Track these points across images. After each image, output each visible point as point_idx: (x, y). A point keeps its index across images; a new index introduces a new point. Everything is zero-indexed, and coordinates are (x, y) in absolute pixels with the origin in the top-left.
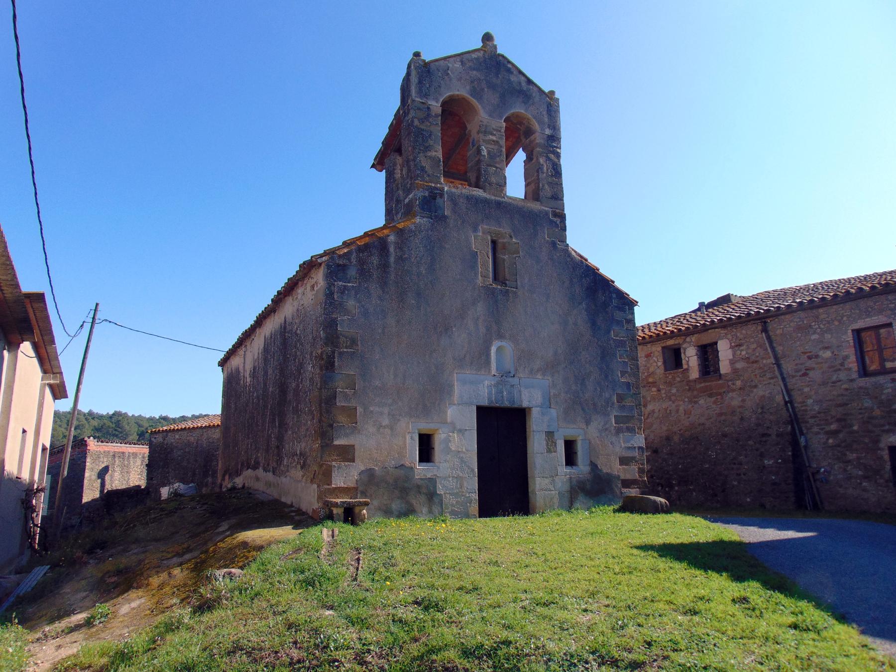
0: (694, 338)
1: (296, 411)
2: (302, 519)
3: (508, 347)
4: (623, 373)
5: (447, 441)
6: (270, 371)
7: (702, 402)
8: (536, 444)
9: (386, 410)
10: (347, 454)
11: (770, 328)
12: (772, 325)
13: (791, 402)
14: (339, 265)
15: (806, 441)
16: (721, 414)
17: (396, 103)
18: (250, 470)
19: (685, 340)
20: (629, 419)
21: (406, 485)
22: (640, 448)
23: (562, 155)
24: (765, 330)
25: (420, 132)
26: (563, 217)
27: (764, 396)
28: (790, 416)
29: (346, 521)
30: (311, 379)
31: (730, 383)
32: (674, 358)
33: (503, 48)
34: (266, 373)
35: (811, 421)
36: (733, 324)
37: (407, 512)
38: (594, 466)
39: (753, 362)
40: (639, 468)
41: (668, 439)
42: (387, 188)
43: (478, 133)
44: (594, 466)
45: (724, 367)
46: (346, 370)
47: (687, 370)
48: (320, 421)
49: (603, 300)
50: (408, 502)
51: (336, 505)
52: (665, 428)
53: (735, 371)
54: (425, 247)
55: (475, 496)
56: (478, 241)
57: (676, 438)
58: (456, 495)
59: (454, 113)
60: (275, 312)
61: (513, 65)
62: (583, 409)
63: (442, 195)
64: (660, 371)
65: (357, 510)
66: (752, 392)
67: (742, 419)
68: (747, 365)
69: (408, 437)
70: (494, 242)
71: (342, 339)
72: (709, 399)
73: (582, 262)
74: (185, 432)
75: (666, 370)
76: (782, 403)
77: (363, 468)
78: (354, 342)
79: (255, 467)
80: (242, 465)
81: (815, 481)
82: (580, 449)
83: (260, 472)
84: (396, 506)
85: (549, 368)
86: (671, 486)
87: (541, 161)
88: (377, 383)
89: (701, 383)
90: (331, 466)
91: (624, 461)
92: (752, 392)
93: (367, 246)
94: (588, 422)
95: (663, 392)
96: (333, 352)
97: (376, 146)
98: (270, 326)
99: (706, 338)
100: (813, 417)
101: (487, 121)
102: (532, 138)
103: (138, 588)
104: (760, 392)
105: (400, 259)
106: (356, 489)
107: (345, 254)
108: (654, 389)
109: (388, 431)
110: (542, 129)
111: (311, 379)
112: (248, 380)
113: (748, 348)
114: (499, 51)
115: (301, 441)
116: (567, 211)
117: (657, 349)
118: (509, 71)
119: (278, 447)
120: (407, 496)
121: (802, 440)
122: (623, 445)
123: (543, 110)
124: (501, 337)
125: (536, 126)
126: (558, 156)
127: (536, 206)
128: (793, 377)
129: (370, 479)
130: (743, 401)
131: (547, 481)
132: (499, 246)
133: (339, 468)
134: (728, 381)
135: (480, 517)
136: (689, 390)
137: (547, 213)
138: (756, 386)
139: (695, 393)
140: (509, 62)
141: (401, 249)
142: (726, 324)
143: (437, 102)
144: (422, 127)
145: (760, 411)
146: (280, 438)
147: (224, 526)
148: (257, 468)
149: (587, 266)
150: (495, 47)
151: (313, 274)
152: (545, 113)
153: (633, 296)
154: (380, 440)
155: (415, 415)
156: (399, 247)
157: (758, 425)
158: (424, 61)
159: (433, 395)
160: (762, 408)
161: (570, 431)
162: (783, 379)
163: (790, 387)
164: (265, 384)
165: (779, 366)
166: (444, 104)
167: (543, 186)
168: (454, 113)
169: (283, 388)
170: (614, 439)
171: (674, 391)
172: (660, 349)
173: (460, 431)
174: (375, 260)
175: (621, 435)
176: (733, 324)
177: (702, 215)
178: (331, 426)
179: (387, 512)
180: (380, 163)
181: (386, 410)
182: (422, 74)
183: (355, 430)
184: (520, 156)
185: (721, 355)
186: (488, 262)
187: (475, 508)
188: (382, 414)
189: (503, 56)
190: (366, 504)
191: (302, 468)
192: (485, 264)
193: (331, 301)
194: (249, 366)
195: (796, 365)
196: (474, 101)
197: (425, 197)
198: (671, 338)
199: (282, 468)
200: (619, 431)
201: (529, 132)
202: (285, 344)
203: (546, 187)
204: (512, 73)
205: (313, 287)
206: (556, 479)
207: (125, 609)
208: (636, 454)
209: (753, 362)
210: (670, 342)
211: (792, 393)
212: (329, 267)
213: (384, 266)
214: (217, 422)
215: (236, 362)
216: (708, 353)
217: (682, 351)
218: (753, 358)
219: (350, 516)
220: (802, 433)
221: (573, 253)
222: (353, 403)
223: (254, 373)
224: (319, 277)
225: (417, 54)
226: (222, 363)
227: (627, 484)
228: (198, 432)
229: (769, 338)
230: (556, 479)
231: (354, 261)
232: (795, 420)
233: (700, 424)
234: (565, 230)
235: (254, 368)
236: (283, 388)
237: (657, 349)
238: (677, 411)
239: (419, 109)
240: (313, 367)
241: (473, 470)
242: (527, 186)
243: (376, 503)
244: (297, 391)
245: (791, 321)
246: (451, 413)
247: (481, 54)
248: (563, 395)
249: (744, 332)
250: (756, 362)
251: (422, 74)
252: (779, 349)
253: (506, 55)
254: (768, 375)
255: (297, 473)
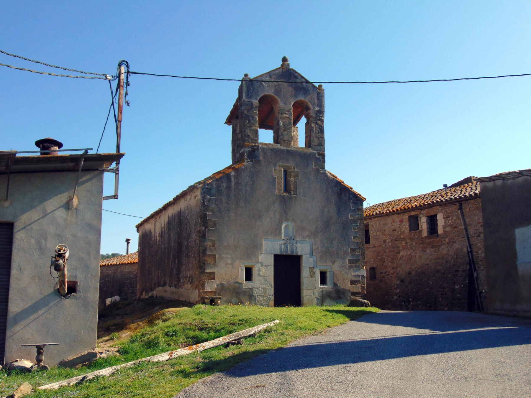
0: (425, 211)
1: (187, 256)
2: (190, 305)
3: (291, 225)
4: (355, 237)
5: (259, 270)
6: (172, 235)
7: (428, 251)
8: (305, 273)
9: (229, 256)
10: (212, 276)
11: (463, 207)
12: (465, 206)
13: (471, 252)
14: (207, 188)
15: (477, 275)
16: (437, 258)
17: (237, 96)
18: (160, 288)
19: (420, 212)
20: (356, 261)
21: (239, 291)
22: (362, 276)
23: (325, 121)
24: (460, 209)
25: (247, 117)
26: (323, 155)
27: (458, 248)
28: (470, 260)
29: (211, 304)
30: (195, 241)
31: (443, 240)
32: (414, 222)
33: (293, 65)
34: (169, 235)
35: (480, 263)
36: (453, 202)
37: (241, 303)
38: (335, 285)
39: (454, 228)
40: (362, 287)
41: (409, 273)
42: (233, 137)
43: (279, 113)
44: (335, 285)
45: (440, 230)
46: (211, 237)
47: (421, 230)
48: (199, 261)
49: (346, 197)
50: (239, 299)
51: (207, 298)
52: (408, 267)
53: (445, 232)
54: (249, 176)
55: (272, 297)
56: (277, 172)
57: (413, 273)
58: (263, 296)
59: (267, 103)
60: (174, 204)
61: (298, 73)
62: (331, 256)
63: (258, 149)
64: (407, 231)
65: (216, 301)
66: (453, 245)
67: (447, 261)
68: (451, 229)
69: (240, 269)
70: (285, 171)
71: (209, 223)
72: (432, 249)
73: (333, 179)
74: (105, 268)
75: (411, 230)
76: (466, 252)
77: (219, 283)
78: (215, 224)
79: (164, 285)
80: (155, 285)
81: (480, 297)
82: (328, 275)
83: (167, 288)
84: (234, 300)
85: (314, 234)
86: (409, 302)
87: (313, 125)
88: (225, 244)
89: (428, 239)
90: (204, 282)
91: (352, 282)
92: (453, 245)
93: (221, 178)
94: (333, 262)
95: (409, 244)
96: (205, 230)
97: (228, 114)
98: (171, 211)
99: (432, 212)
100: (481, 261)
101: (286, 105)
102: (309, 111)
103: (126, 329)
104: (457, 246)
105: (237, 184)
106: (215, 292)
107: (210, 183)
108: (404, 242)
109: (230, 266)
110: (314, 108)
111: (195, 241)
112: (158, 238)
113: (452, 219)
114: (291, 67)
115: (190, 271)
116: (326, 152)
117: (406, 217)
118: (296, 77)
119: (177, 274)
120: (239, 295)
121: (475, 274)
122: (353, 274)
123: (315, 97)
124: (287, 220)
125: (311, 106)
126: (323, 121)
127: (310, 151)
128: (473, 237)
129: (222, 288)
130: (448, 250)
131: (310, 291)
132: (288, 174)
133: (208, 282)
134: (442, 238)
135: (275, 306)
136: (422, 243)
137: (314, 154)
138: (455, 242)
139: (425, 245)
140: (296, 72)
141: (237, 178)
142: (440, 204)
143: (256, 100)
144: (248, 114)
145: (455, 257)
146: (179, 270)
147: (157, 308)
148: (165, 285)
149: (337, 181)
150: (289, 65)
151: (195, 190)
152: (316, 98)
153: (363, 195)
154: (226, 270)
155: (245, 257)
156: (236, 177)
157: (454, 265)
158: (250, 78)
159: (254, 248)
160: (457, 255)
161: (324, 268)
162: (468, 238)
163: (471, 242)
164: (169, 241)
165: (466, 229)
166: (260, 101)
167: (313, 139)
168: (267, 103)
169: (180, 244)
170: (347, 271)
171: (414, 244)
172: (407, 217)
173: (266, 266)
174: (225, 185)
175: (352, 270)
176: (453, 202)
177: (396, 155)
178: (204, 263)
179: (229, 302)
180: (229, 121)
181: (229, 256)
182: (248, 85)
183: (215, 265)
184: (303, 120)
185: (439, 222)
186: (281, 182)
187: (272, 302)
188: (227, 258)
189: (293, 70)
190: (220, 298)
191: (190, 283)
192: (280, 184)
193: (204, 206)
194: (158, 231)
195: (475, 230)
196: (276, 97)
197: (249, 151)
198: (413, 211)
199: (180, 284)
200: (350, 267)
201: (308, 108)
202: (180, 222)
203: (315, 139)
204: (298, 78)
205: (195, 197)
206: (315, 291)
207: (123, 335)
208: (360, 279)
209: (454, 228)
210: (413, 213)
211: (472, 247)
212: (202, 189)
213: (229, 188)
214: (136, 259)
215: (148, 227)
216: (432, 221)
217: (419, 219)
218: (455, 225)
219: (212, 302)
220: (475, 270)
221: (329, 175)
222: (214, 253)
223: (162, 235)
224: (198, 193)
225: (246, 75)
226: (138, 227)
227: (353, 294)
228: (114, 268)
229: (462, 213)
230: (315, 291)
231: (214, 186)
232: (472, 263)
233: (426, 265)
234: (325, 162)
235: (162, 232)
236: (180, 244)
237: (406, 217)
238: (415, 256)
239: (247, 105)
240: (196, 236)
241: (271, 285)
242: (306, 137)
243: (225, 299)
244: (187, 247)
245: (474, 204)
246: (261, 258)
247: (281, 70)
248: (320, 249)
249: (450, 209)
250: (456, 227)
251: (248, 85)
252: (467, 220)
253: (294, 69)
254: (461, 236)
255: (189, 286)
